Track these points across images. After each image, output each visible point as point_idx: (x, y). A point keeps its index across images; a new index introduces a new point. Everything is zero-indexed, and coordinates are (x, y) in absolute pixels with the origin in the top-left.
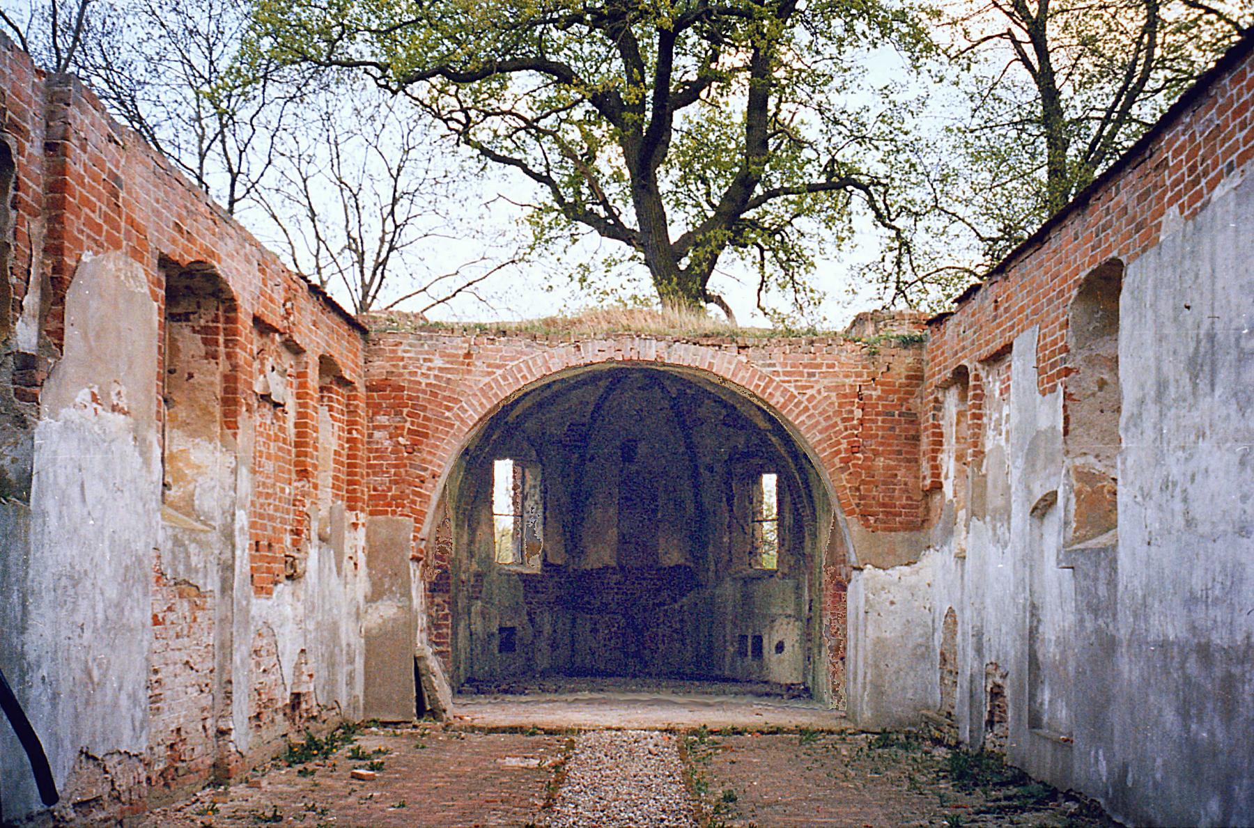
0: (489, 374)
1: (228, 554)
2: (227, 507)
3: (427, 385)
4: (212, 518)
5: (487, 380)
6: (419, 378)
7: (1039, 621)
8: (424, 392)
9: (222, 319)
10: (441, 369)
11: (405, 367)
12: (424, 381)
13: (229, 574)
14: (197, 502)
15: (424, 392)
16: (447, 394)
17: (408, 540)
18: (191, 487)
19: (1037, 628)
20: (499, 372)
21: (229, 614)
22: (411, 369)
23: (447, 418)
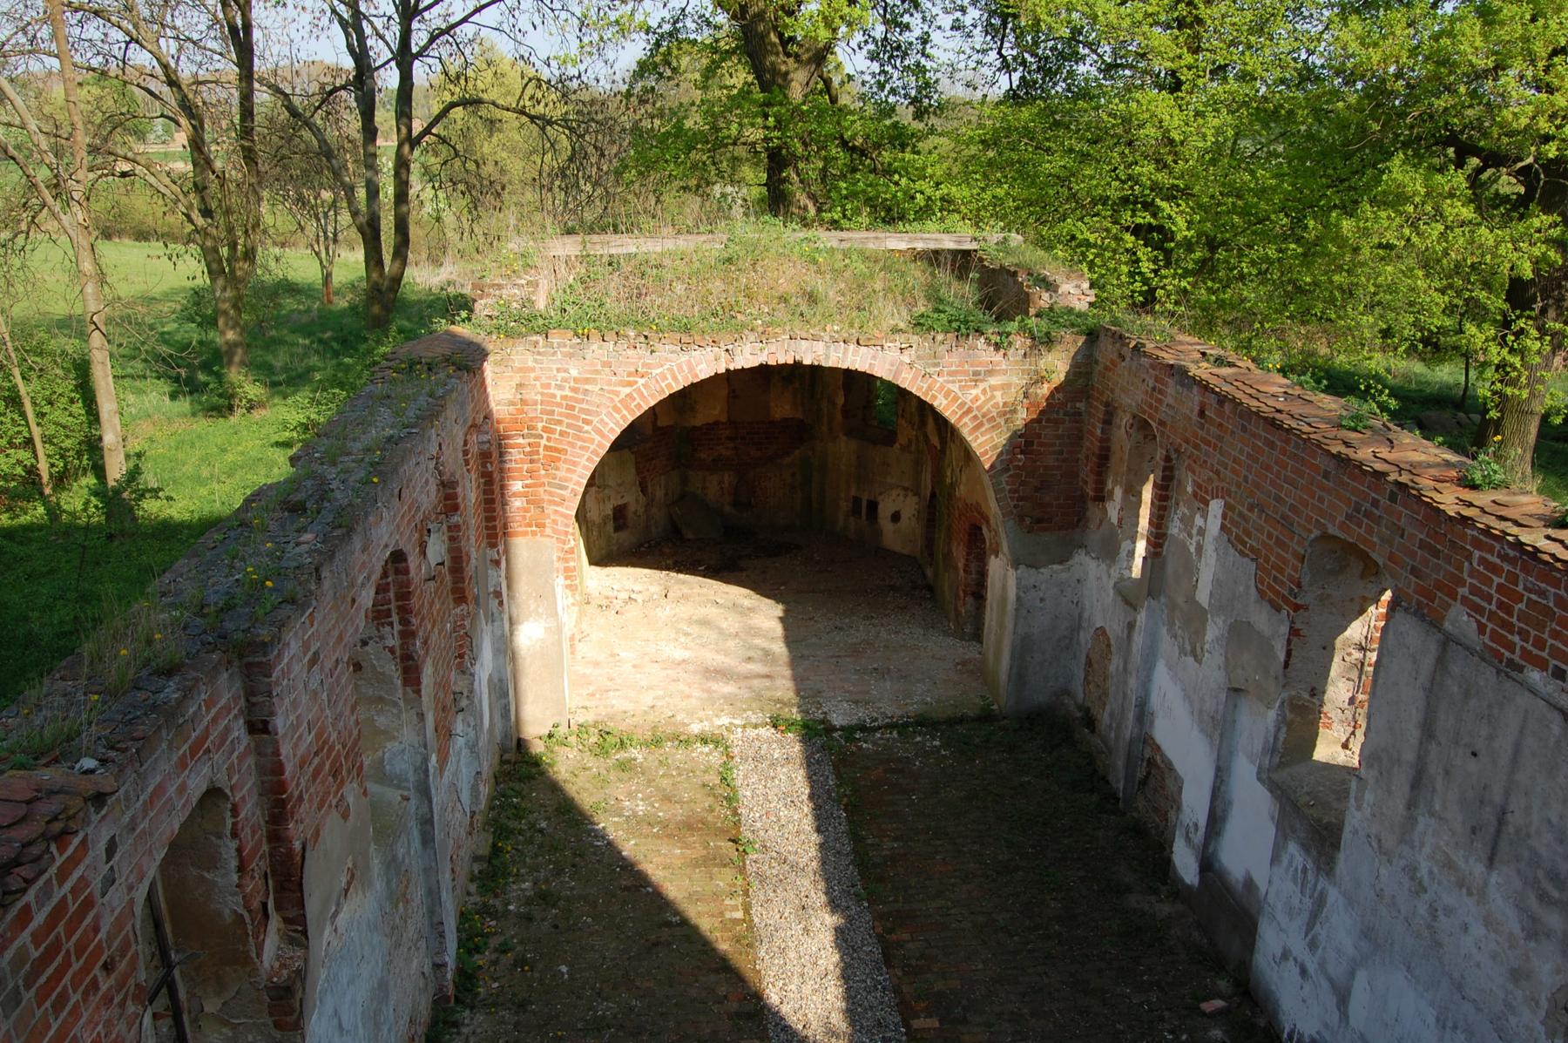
0: (630, 384)
1: (425, 809)
2: (418, 764)
3: (563, 397)
4: (407, 780)
5: (628, 390)
6: (552, 391)
7: (1222, 781)
8: (559, 405)
9: (391, 572)
10: (576, 380)
11: (537, 379)
12: (559, 393)
13: (428, 827)
14: (388, 767)
15: (559, 405)
16: (584, 406)
17: (552, 562)
18: (380, 753)
19: (1219, 788)
20: (641, 381)
21: (433, 864)
22: (544, 380)
23: (587, 432)
